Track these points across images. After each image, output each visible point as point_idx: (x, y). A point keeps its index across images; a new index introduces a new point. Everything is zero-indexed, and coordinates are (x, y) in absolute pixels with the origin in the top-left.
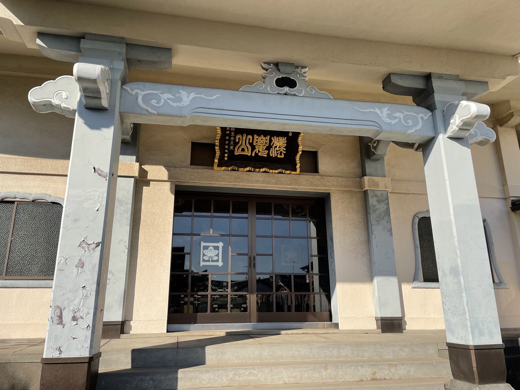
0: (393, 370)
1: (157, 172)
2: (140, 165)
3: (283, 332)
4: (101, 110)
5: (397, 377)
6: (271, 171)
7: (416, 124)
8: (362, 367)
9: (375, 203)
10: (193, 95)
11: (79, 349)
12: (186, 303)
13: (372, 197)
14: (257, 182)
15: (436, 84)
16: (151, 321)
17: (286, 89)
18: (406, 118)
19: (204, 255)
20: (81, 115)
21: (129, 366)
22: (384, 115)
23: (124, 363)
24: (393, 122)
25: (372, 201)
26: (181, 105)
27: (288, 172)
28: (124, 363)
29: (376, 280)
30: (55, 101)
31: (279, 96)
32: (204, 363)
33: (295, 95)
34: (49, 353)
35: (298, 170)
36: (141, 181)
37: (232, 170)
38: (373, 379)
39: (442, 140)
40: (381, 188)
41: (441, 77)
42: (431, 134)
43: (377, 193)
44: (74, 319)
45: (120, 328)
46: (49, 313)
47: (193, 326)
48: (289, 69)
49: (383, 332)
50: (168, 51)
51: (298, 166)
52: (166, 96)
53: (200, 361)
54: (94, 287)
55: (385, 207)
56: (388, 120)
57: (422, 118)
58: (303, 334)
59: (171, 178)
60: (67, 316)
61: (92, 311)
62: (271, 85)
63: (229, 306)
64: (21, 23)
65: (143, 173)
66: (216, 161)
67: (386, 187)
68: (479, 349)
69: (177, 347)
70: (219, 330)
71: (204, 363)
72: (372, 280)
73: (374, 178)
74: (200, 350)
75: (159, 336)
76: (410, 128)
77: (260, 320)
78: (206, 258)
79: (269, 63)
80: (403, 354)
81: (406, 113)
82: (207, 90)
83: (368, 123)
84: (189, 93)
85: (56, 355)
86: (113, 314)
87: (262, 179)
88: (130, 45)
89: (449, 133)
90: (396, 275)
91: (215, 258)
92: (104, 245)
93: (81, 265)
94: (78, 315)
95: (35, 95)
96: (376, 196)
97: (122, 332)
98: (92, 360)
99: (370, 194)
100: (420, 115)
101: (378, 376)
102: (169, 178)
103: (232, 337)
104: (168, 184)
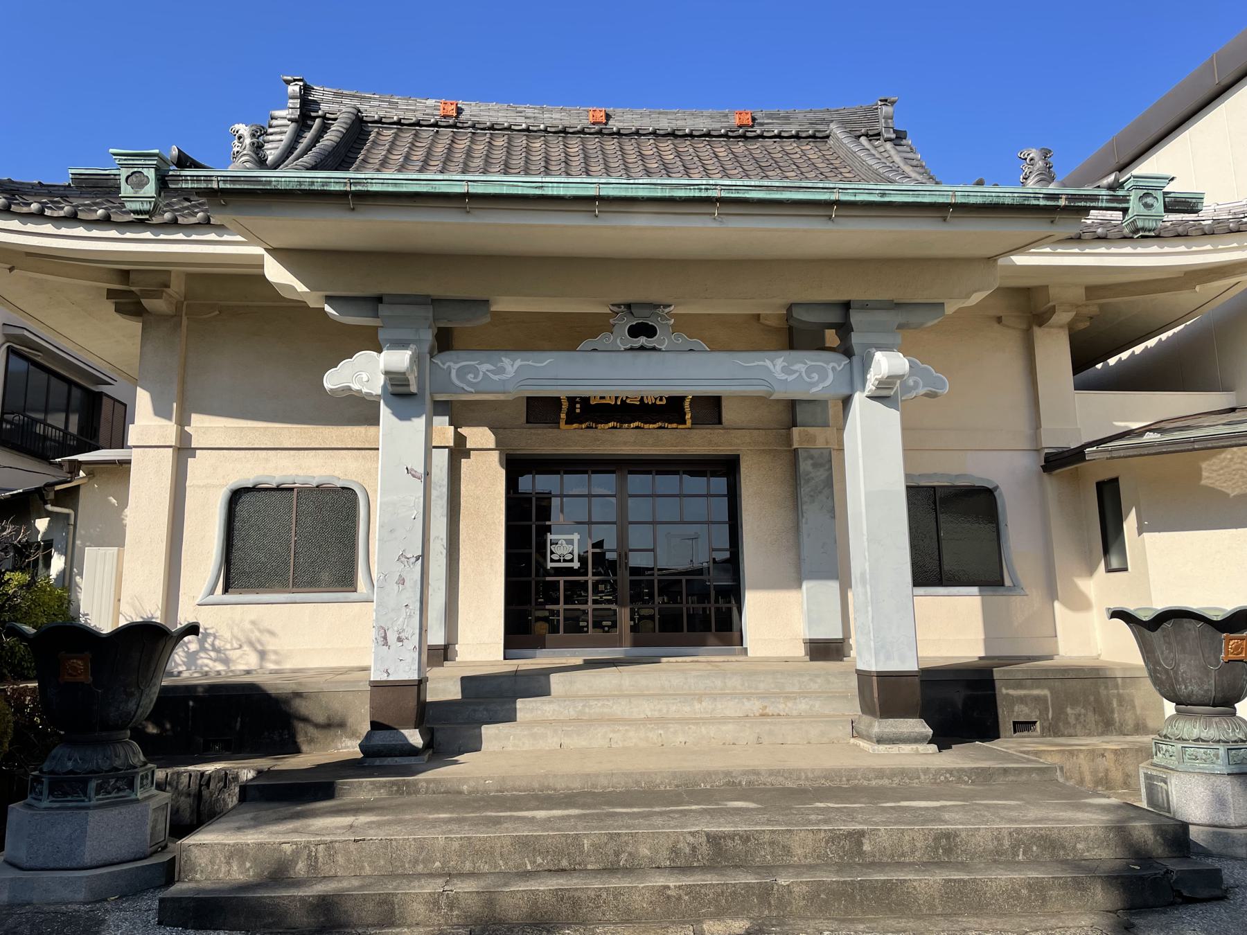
0: (790, 704)
2: (456, 429)
3: (664, 660)
4: (411, 395)
5: (795, 713)
6: (646, 426)
7: (823, 378)
8: (748, 699)
9: (809, 468)
10: (518, 363)
11: (406, 671)
13: (805, 459)
14: (625, 443)
15: (856, 318)
16: (482, 642)
17: (643, 340)
18: (809, 371)
19: (552, 553)
20: (387, 404)
21: (459, 697)
22: (778, 368)
23: (454, 692)
25: (805, 466)
26: (503, 377)
27: (674, 425)
28: (454, 692)
29: (805, 585)
30: (355, 387)
31: (630, 354)
32: (549, 694)
33: (654, 349)
34: (376, 676)
35: (689, 423)
36: (459, 451)
38: (762, 715)
39: (859, 399)
40: (820, 443)
41: (865, 306)
42: (846, 392)
43: (813, 452)
44: (400, 640)
45: (442, 654)
46: (373, 633)
47: (539, 652)
48: (646, 312)
49: (812, 660)
50: (486, 302)
51: (688, 416)
52: (485, 367)
53: (544, 691)
54: (418, 604)
55: (827, 473)
56: (783, 376)
57: (834, 369)
59: (499, 445)
60: (392, 637)
61: (417, 631)
62: (621, 338)
64: (306, 289)
65: (460, 439)
66: (563, 416)
67: (827, 443)
68: (882, 675)
69: (516, 675)
70: (575, 657)
71: (549, 694)
72: (800, 586)
73: (809, 429)
74: (542, 678)
75: (493, 663)
77: (636, 644)
78: (555, 557)
79: (618, 305)
80: (814, 687)
82: (536, 354)
83: (755, 382)
84: (514, 361)
85: (384, 677)
86: (437, 637)
87: (632, 440)
88: (436, 302)
89: (866, 393)
92: (424, 557)
93: (402, 581)
94: (403, 635)
95: (333, 379)
96: (812, 457)
97: (446, 659)
98: (421, 683)
99: (802, 454)
100: (832, 364)
101: (769, 711)
102: (498, 442)
103: (590, 664)
104: (496, 454)
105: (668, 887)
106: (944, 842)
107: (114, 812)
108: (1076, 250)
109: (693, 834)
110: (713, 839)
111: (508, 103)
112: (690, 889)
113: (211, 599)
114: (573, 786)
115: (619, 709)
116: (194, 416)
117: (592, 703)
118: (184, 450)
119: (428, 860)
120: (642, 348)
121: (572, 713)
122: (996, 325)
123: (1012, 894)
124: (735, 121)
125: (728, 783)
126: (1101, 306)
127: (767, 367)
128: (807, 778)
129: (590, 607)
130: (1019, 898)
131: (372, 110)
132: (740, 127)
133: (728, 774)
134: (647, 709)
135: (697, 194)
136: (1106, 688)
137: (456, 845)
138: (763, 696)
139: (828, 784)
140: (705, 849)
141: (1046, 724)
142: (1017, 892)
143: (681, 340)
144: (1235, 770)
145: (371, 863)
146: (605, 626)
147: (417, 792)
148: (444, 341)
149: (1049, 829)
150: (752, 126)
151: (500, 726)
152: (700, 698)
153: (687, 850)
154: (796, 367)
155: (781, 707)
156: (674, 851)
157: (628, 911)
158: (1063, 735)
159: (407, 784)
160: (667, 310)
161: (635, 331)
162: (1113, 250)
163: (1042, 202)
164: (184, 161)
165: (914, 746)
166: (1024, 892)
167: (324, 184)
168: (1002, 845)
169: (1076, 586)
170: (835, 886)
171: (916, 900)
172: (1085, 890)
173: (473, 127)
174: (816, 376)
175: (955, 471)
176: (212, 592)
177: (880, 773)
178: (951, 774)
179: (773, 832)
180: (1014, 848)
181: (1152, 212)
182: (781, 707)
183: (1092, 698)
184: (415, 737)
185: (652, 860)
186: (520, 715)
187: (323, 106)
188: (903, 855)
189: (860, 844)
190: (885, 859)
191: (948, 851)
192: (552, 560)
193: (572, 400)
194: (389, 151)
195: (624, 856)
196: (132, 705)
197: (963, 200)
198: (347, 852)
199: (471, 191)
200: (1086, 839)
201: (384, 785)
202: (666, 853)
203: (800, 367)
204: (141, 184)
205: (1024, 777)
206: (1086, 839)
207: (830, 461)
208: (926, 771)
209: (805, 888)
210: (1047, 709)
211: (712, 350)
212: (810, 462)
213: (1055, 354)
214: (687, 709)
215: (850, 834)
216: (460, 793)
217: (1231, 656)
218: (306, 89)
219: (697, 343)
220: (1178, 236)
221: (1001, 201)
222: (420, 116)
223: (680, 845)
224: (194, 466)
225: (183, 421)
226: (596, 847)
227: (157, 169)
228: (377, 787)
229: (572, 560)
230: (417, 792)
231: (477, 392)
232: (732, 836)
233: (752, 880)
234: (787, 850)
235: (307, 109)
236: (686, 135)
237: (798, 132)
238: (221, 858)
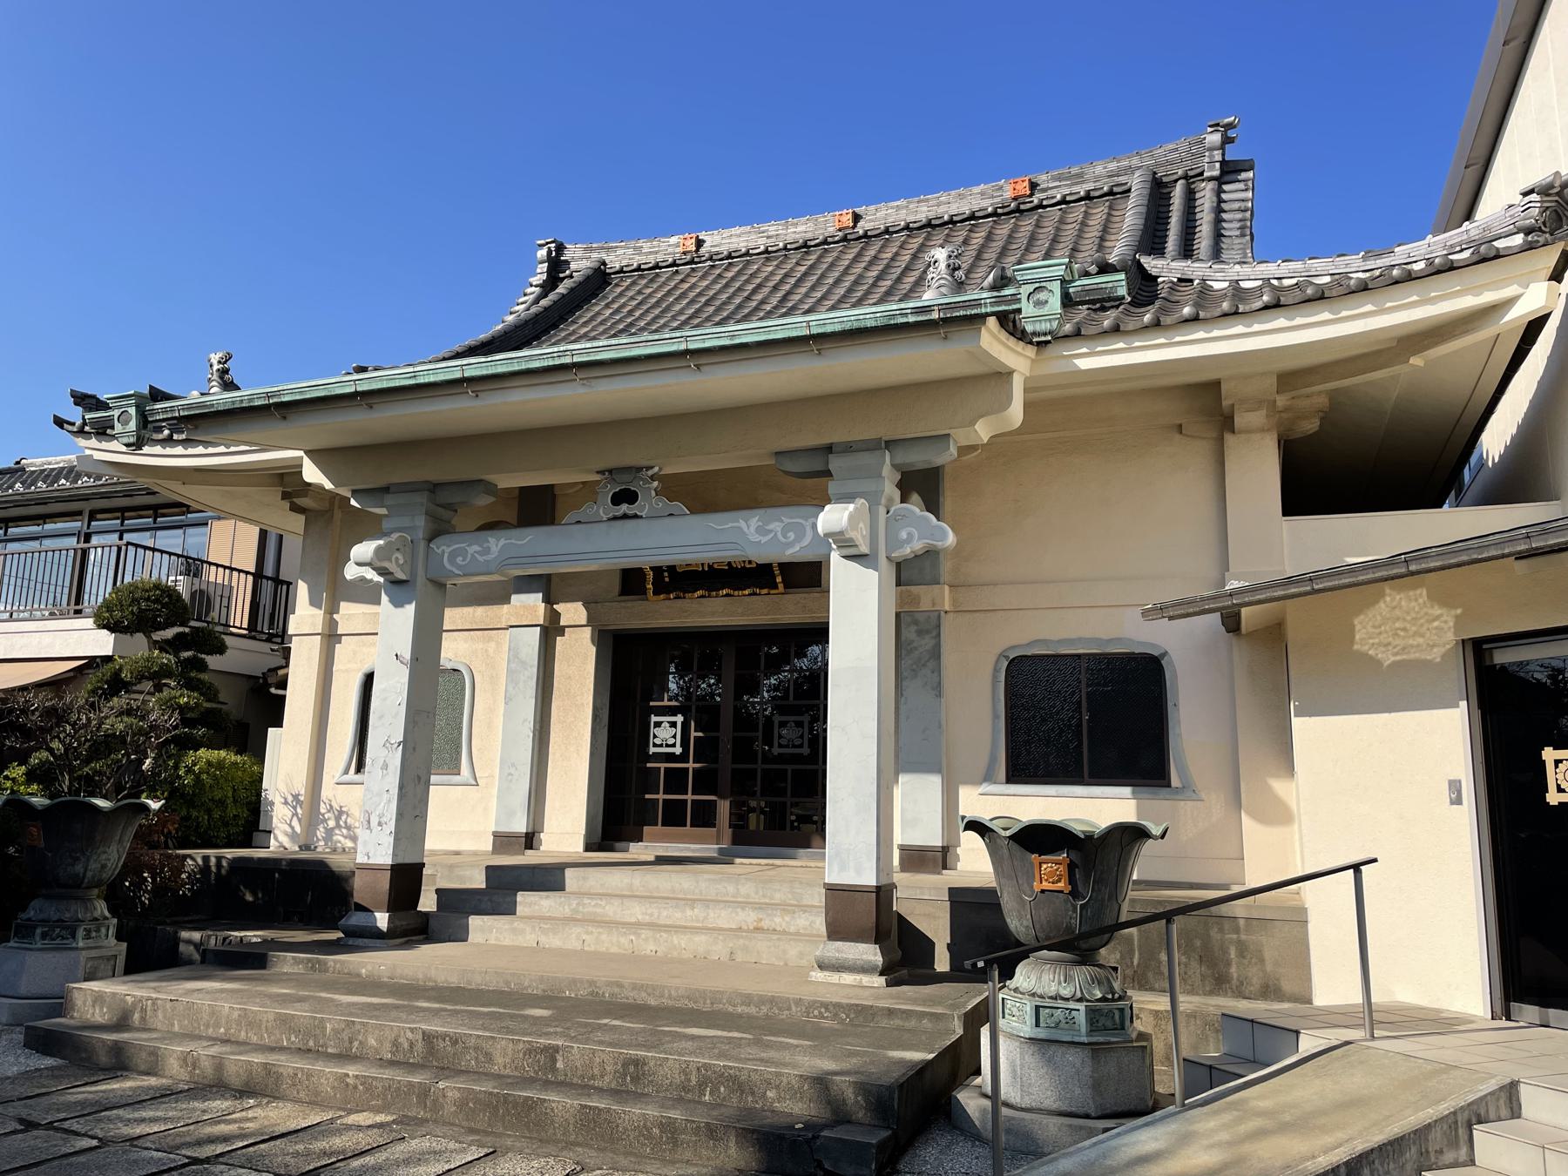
1: (572, 612)
3: (738, 860)
5: (792, 929)
10: (502, 542)
12: (753, 810)
14: (713, 614)
16: (566, 828)
17: (624, 508)
19: (780, 737)
22: (752, 529)
24: (764, 539)
33: (636, 516)
36: (551, 631)
38: (757, 929)
41: (849, 448)
43: (917, 616)
48: (626, 477)
51: (779, 579)
56: (755, 538)
58: (661, 861)
60: (374, 821)
62: (604, 509)
65: (554, 617)
73: (912, 588)
78: (658, 741)
81: (786, 520)
91: (671, 741)
93: (385, 766)
94: (384, 820)
96: (916, 623)
97: (945, 867)
101: (766, 924)
104: (588, 630)
106: (632, 1068)
107: (49, 956)
108: (1162, 341)
109: (412, 1030)
110: (428, 1037)
111: (751, 224)
113: (346, 778)
115: (612, 910)
117: (586, 901)
118: (331, 637)
120: (625, 517)
121: (567, 911)
122: (1178, 436)
123: (644, 1130)
125: (592, 993)
126: (1333, 395)
128: (670, 997)
129: (689, 797)
130: (650, 1137)
131: (614, 261)
132: (1015, 199)
133: (592, 983)
134: (636, 912)
135: (551, 363)
136: (1221, 930)
137: (236, 1014)
139: (691, 1005)
140: (420, 1046)
141: (1129, 972)
143: (661, 504)
144: (1041, 1033)
147: (326, 971)
148: (439, 529)
149: (740, 1070)
150: (1031, 195)
151: (486, 918)
152: (692, 902)
153: (406, 1045)
154: (771, 527)
155: (779, 921)
156: (396, 1044)
157: (317, 1094)
159: (319, 961)
160: (650, 473)
161: (617, 499)
162: (1216, 333)
163: (911, 319)
164: (157, 395)
165: (858, 977)
166: (656, 1131)
167: (250, 400)
169: (1269, 789)
171: (553, 1122)
173: (711, 259)
175: (1104, 634)
176: (346, 772)
177: (748, 1000)
178: (827, 1009)
180: (702, 1085)
181: (1045, 310)
182: (779, 921)
183: (1198, 943)
184: (382, 920)
185: (377, 1051)
187: (573, 266)
188: (593, 1077)
189: (554, 1061)
190: (575, 1080)
191: (636, 1079)
192: (655, 745)
193: (657, 570)
194: (901, 247)
195: (356, 1044)
196: (79, 868)
197: (820, 330)
198: (165, 1011)
200: (777, 1087)
201: (301, 961)
202: (388, 1046)
203: (776, 526)
204: (126, 423)
205: (913, 1023)
207: (939, 626)
209: (457, 1095)
210: (1131, 952)
211: (692, 513)
212: (913, 628)
213: (1258, 471)
214: (679, 915)
215: (546, 1049)
216: (359, 975)
217: (1046, 885)
218: (560, 248)
219: (679, 506)
220: (1397, 282)
221: (862, 325)
222: (660, 258)
223: (401, 1040)
224: (340, 650)
225: (332, 610)
226: (336, 1031)
227: (137, 407)
228: (297, 962)
229: (674, 745)
230: (326, 971)
232: (444, 1036)
233: (652, 1112)
234: (489, 1057)
235: (556, 266)
237: (1064, 197)
238: (89, 1002)
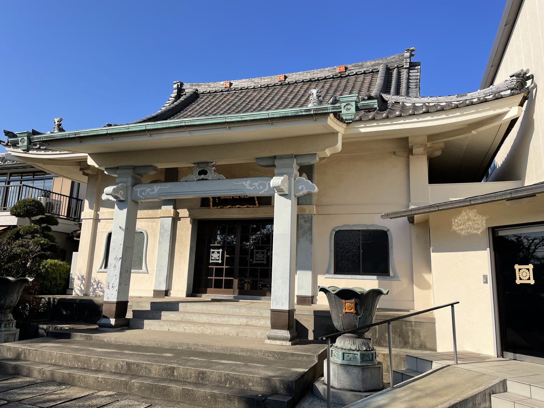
0: (257, 321)
1: (184, 212)
3: (240, 301)
5: (259, 325)
8: (242, 318)
10: (159, 187)
14: (234, 214)
18: (259, 186)
19: (256, 257)
22: (248, 185)
24: (252, 188)
33: (207, 179)
36: (176, 219)
37: (221, 208)
40: (307, 212)
41: (282, 157)
48: (204, 165)
51: (257, 202)
53: (176, 309)
55: (310, 225)
56: (249, 188)
59: (190, 216)
60: (111, 286)
63: (364, 283)
65: (177, 214)
76: (261, 190)
78: (213, 258)
81: (260, 182)
88: (134, 168)
90: (311, 270)
93: (115, 267)
94: (114, 286)
96: (304, 218)
97: (312, 303)
101: (249, 323)
104: (189, 219)
105: (98, 378)
106: (201, 375)
108: (389, 123)
109: (122, 361)
110: (128, 364)
111: (249, 78)
112: (104, 379)
114: (137, 343)
115: (195, 318)
116: (101, 208)
117: (186, 315)
118: (97, 220)
119: (52, 359)
120: (203, 179)
121: (179, 318)
122: (394, 156)
123: (205, 398)
124: (338, 71)
125: (187, 348)
126: (446, 143)
127: (243, 184)
128: (215, 349)
130: (207, 399)
131: (201, 89)
133: (188, 344)
135: (177, 125)
136: (406, 326)
138: (247, 317)
141: (375, 340)
142: (207, 397)
143: (216, 175)
144: (345, 362)
145: (38, 358)
146: (229, 285)
148: (136, 182)
150: (345, 72)
151: (150, 320)
152: (224, 315)
153: (120, 367)
155: (254, 322)
156: (116, 366)
157: (87, 384)
158: (382, 346)
159: (89, 336)
160: (212, 164)
161: (200, 173)
163: (304, 113)
164: (35, 133)
165: (282, 342)
168: (221, 379)
169: (423, 277)
170: (147, 385)
171: (172, 394)
172: (231, 400)
173: (235, 90)
174: (261, 187)
175: (369, 223)
176: (101, 268)
177: (243, 350)
179: (146, 364)
180: (226, 381)
181: (350, 112)
182: (254, 322)
183: (398, 330)
184: (113, 321)
185: (110, 369)
186: (163, 318)
187: (186, 91)
188: (187, 378)
189: (173, 372)
190: (181, 379)
191: (202, 379)
192: (212, 260)
193: (214, 198)
195: (102, 366)
198: (33, 353)
199: (108, 132)
200: (253, 382)
202: (113, 367)
203: (256, 184)
204: (24, 142)
205: (300, 358)
206: (253, 382)
208: (261, 351)
209: (138, 384)
210: (376, 333)
213: (420, 168)
214: (219, 320)
215: (171, 368)
216: (104, 341)
217: (347, 311)
218: (182, 84)
220: (468, 105)
221: (287, 115)
225: (97, 210)
226: (95, 362)
227: (28, 137)
228: (81, 336)
229: (219, 260)
231: (145, 199)
232: (134, 364)
234: (150, 371)
235: (180, 91)
236: (316, 80)
